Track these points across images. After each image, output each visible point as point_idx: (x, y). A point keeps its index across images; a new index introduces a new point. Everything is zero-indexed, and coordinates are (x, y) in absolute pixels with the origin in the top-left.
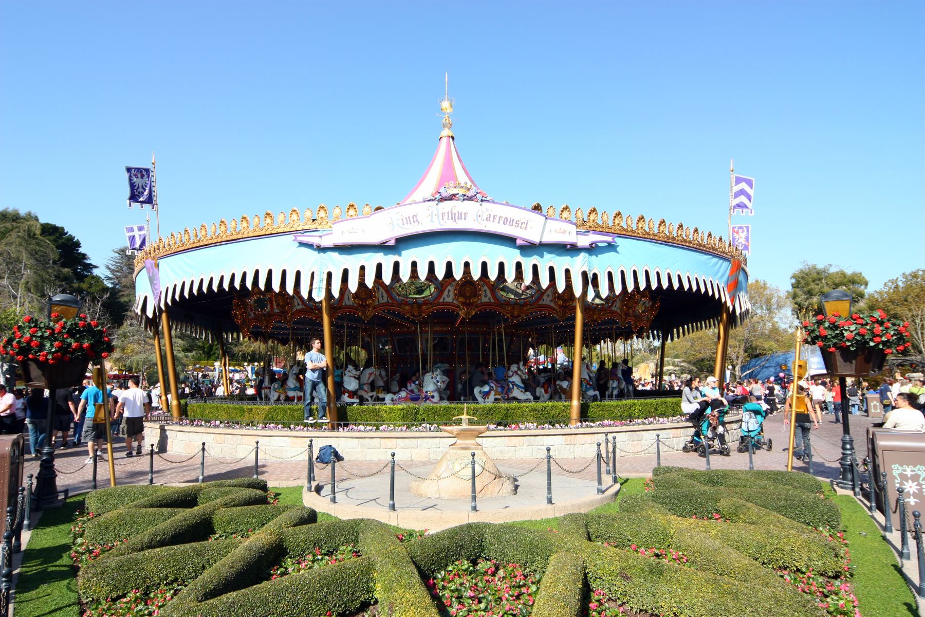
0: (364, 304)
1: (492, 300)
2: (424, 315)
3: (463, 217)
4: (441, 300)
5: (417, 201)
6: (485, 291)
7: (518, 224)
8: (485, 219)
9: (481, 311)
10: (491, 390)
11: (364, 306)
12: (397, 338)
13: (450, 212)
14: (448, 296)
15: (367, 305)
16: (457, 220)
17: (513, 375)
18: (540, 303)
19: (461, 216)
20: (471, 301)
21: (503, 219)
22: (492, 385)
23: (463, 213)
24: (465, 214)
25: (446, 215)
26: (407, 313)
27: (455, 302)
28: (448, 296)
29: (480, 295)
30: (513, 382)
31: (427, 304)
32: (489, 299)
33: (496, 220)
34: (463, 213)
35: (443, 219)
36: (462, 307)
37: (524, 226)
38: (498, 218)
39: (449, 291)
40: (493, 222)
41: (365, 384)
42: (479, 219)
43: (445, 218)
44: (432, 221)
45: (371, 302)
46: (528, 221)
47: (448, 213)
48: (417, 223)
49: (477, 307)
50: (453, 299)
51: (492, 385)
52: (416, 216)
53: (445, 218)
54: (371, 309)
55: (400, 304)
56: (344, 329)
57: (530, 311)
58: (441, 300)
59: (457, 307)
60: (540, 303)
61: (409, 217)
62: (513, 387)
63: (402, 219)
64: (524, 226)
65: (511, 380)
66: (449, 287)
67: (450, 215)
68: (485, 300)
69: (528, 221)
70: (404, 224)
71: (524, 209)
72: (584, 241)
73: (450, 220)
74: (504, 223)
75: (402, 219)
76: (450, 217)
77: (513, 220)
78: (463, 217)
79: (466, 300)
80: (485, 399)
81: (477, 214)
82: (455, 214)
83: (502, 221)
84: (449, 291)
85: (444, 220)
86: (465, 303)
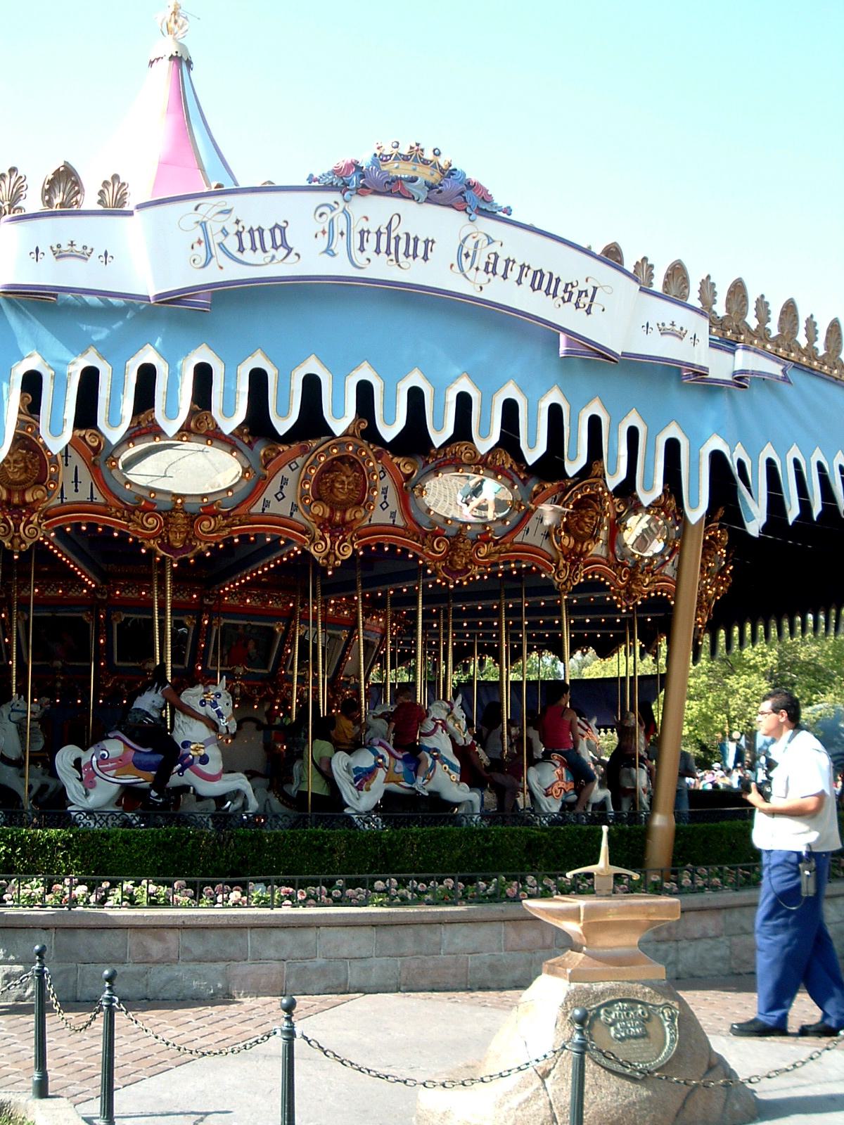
0: (16, 500)
1: (399, 522)
2: (201, 546)
3: (421, 252)
4: (257, 509)
5: (278, 184)
6: (385, 491)
7: (571, 294)
8: (482, 267)
9: (366, 547)
10: (378, 765)
11: (17, 507)
12: (224, 621)
13: (383, 230)
14: (280, 497)
15: (24, 504)
16: (401, 257)
17: (434, 731)
18: (518, 539)
19: (419, 248)
20: (348, 516)
21: (531, 274)
22: (381, 751)
23: (422, 238)
24: (426, 242)
25: (373, 238)
26: (149, 538)
27: (296, 516)
28: (280, 497)
29: (371, 501)
30: (435, 750)
31: (214, 515)
32: (393, 515)
33: (514, 274)
34: (422, 238)
35: (362, 249)
36: (318, 532)
37: (585, 300)
38: (517, 269)
39: (284, 481)
40: (505, 277)
41: (379, 892)
42: (466, 263)
43: (370, 246)
44: (329, 251)
45: (39, 494)
46: (595, 289)
47: (379, 233)
48: (282, 252)
49: (359, 537)
50: (295, 507)
51: (381, 751)
52: (283, 230)
53: (370, 246)
54: (35, 518)
55: (132, 511)
56: (560, 613)
57: (494, 559)
58: (257, 509)
59: (304, 533)
60: (518, 539)
61: (261, 230)
62: (434, 766)
63: (239, 234)
64: (585, 300)
65: (431, 746)
66: (286, 471)
67: (384, 238)
68: (380, 517)
69: (595, 289)
70: (241, 249)
71: (587, 252)
72: (721, 366)
73: (383, 255)
74: (532, 285)
75: (239, 234)
76: (383, 247)
77: (558, 280)
78: (421, 252)
79: (333, 511)
80: (359, 788)
81: (461, 247)
82: (398, 238)
83: (527, 281)
84: (284, 481)
85: (367, 254)
86: (330, 519)
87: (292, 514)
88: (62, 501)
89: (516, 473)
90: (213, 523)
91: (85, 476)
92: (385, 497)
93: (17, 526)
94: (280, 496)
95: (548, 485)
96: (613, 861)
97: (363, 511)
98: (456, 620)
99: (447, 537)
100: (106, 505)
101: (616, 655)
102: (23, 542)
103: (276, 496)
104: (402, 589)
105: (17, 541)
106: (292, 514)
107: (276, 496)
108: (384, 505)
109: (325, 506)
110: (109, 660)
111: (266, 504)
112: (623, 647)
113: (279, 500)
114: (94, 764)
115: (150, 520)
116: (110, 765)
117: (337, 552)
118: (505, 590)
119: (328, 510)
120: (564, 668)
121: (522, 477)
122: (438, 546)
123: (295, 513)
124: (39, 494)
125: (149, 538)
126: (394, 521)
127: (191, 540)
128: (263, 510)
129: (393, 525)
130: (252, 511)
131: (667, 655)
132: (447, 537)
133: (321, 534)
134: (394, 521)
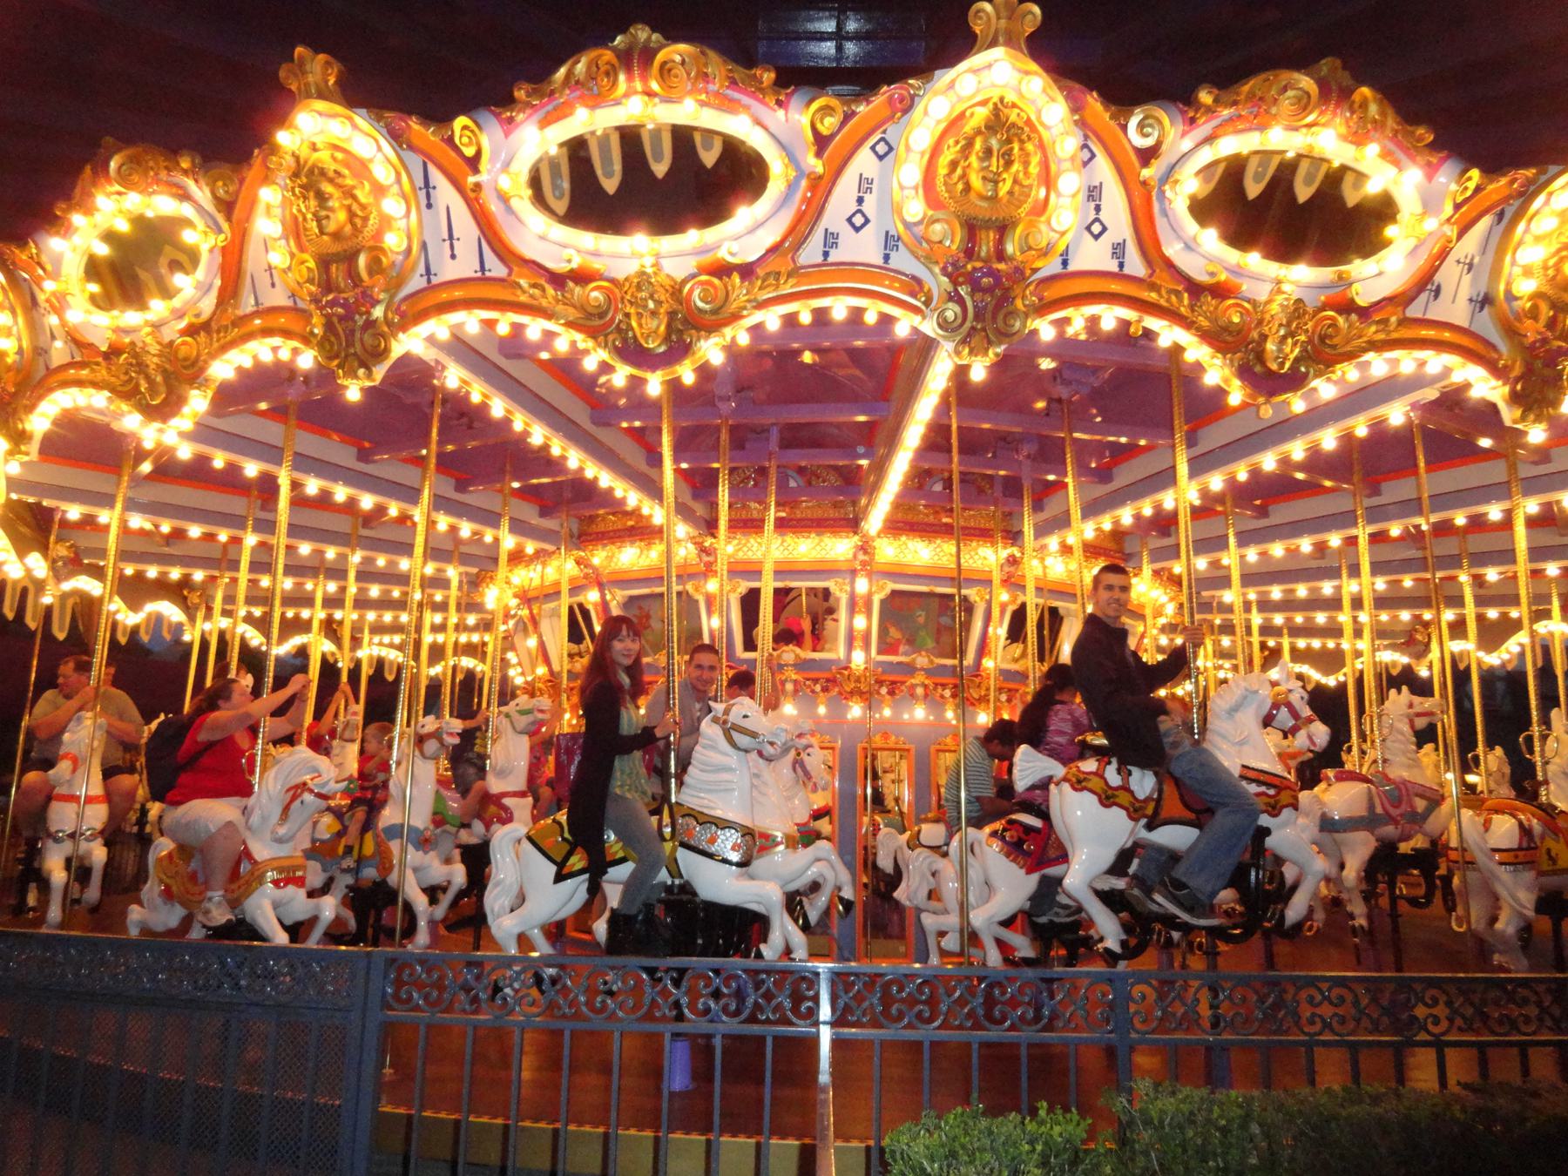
1: (1135, 265)
32: (1118, 250)
87: (887, 258)
88: (429, 281)
92: (1098, 208)
94: (858, 220)
96: (1355, 524)
101: (1500, 383)
103: (849, 220)
104: (799, 352)
106: (887, 258)
107: (849, 220)
108: (1096, 228)
111: (831, 240)
112: (598, 628)
113: (857, 229)
120: (300, 829)
123: (893, 254)
126: (1121, 265)
127: (680, 332)
128: (826, 254)
129: (1119, 276)
131: (1426, 284)
134: (1121, 265)
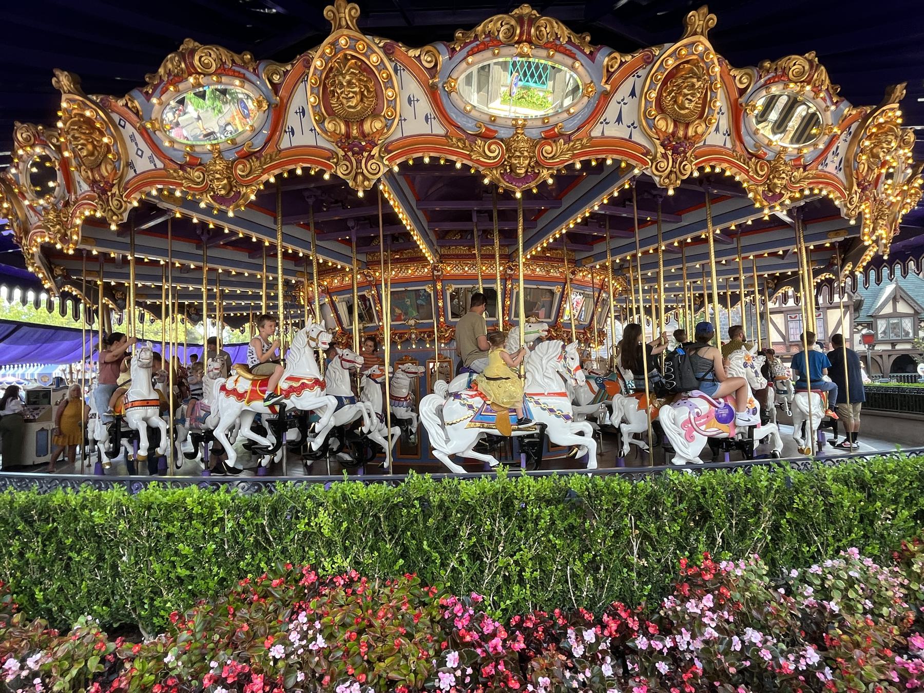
20: (691, 132)
54: (375, 151)
56: (129, 278)
60: (596, 133)
89: (578, 48)
90: (555, 148)
91: (424, 106)
93: (359, 162)
95: (628, 58)
97: (704, 126)
98: (718, 259)
99: (502, 140)
100: (446, 136)
102: (366, 178)
105: (360, 178)
109: (669, 122)
110: (445, 316)
114: (693, 421)
115: (493, 147)
116: (702, 421)
117: (365, 171)
118: (499, 211)
119: (672, 126)
121: (587, 51)
122: (493, 152)
124: (378, 125)
125: (490, 167)
130: (593, 134)
132: (502, 140)
133: (663, 151)
